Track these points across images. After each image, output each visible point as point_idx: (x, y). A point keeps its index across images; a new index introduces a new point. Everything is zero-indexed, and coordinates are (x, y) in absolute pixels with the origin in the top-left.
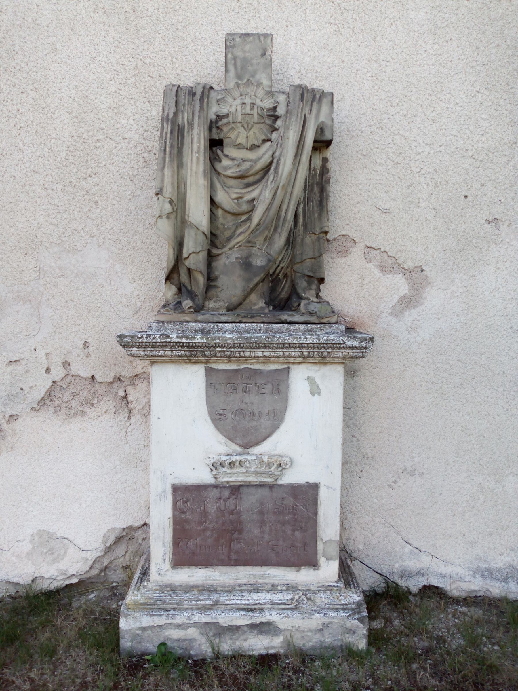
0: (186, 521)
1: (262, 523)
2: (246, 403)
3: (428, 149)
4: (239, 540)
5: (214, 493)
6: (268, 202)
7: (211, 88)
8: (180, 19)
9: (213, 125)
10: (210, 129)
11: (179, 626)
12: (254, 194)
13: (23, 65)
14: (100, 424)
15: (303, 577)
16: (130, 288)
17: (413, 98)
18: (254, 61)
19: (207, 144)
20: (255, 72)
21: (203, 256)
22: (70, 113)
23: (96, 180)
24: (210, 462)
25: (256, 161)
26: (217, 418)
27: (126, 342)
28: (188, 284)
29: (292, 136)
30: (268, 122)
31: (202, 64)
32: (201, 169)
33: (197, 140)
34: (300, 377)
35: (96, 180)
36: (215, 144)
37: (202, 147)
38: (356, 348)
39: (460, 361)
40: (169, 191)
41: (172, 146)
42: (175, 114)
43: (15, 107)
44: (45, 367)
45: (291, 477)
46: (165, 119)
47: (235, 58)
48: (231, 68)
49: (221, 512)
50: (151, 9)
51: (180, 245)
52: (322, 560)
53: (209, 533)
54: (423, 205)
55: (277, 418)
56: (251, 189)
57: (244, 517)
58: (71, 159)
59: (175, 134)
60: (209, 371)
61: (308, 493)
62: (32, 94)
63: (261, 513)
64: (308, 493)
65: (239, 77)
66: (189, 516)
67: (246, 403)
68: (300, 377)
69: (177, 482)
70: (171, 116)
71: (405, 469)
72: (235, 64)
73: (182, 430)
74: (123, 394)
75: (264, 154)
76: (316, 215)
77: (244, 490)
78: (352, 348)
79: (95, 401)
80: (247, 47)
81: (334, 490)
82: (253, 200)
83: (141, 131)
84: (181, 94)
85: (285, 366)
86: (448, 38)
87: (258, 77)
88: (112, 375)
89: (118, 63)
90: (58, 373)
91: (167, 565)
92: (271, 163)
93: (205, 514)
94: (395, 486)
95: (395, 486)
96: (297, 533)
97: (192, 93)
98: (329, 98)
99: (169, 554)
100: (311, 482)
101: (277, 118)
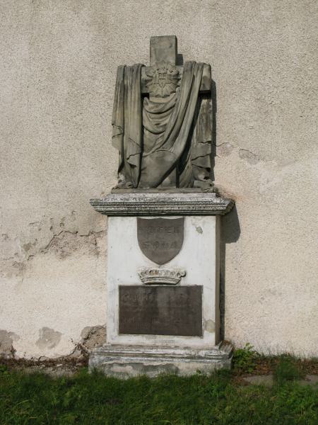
0: (127, 307)
1: (170, 309)
2: (160, 234)
3: (275, 90)
4: (156, 319)
5: (143, 291)
6: (172, 126)
7: (143, 66)
8: (129, 25)
9: (143, 84)
10: (141, 88)
11: (121, 365)
12: (167, 121)
13: (43, 56)
14: (82, 261)
15: (193, 342)
16: (101, 179)
17: (265, 61)
18: (166, 51)
19: (140, 96)
20: (166, 57)
21: (137, 156)
22: (68, 80)
23: (81, 117)
24: (139, 272)
25: (166, 104)
26: (144, 246)
27: (95, 203)
28: (132, 175)
29: (186, 90)
30: (174, 82)
31: (139, 53)
32: (136, 110)
33: (134, 95)
34: (190, 222)
35: (81, 117)
36: (144, 95)
37: (137, 99)
38: (219, 204)
39: (302, 219)
40: (119, 123)
41: (120, 99)
42: (123, 81)
43: (38, 79)
44: (50, 226)
45: (189, 281)
46: (117, 84)
47: (155, 50)
48: (153, 55)
49: (147, 302)
50: (113, 21)
51: (123, 153)
52: (205, 333)
53: (139, 315)
54: (275, 123)
55: (177, 246)
56: (164, 119)
57: (159, 305)
58: (67, 106)
59: (122, 90)
60: (139, 221)
61: (196, 291)
62: (47, 71)
63: (169, 303)
64: (196, 291)
65: (157, 59)
66: (128, 304)
67: (160, 234)
68: (190, 222)
69: (122, 284)
70: (120, 82)
71: (270, 290)
72: (155, 53)
73: (124, 257)
74: (94, 238)
75: (170, 101)
76: (204, 132)
77: (157, 289)
78: (217, 204)
79: (78, 247)
80: (162, 44)
81: (211, 290)
82: (165, 125)
83: (107, 88)
84: (127, 70)
85: (181, 217)
86: (285, 25)
87: (168, 58)
88: (88, 231)
89: (94, 51)
90: (57, 230)
91: (116, 332)
92: (174, 106)
93: (137, 303)
94: (263, 302)
95: (263, 302)
96: (190, 316)
97: (132, 69)
98: (208, 67)
99: (117, 327)
100: (198, 284)
101: (179, 80)
